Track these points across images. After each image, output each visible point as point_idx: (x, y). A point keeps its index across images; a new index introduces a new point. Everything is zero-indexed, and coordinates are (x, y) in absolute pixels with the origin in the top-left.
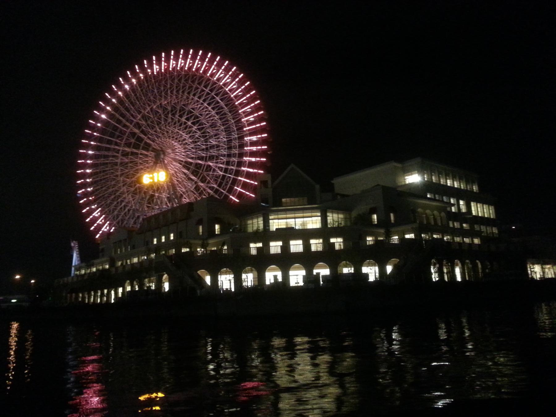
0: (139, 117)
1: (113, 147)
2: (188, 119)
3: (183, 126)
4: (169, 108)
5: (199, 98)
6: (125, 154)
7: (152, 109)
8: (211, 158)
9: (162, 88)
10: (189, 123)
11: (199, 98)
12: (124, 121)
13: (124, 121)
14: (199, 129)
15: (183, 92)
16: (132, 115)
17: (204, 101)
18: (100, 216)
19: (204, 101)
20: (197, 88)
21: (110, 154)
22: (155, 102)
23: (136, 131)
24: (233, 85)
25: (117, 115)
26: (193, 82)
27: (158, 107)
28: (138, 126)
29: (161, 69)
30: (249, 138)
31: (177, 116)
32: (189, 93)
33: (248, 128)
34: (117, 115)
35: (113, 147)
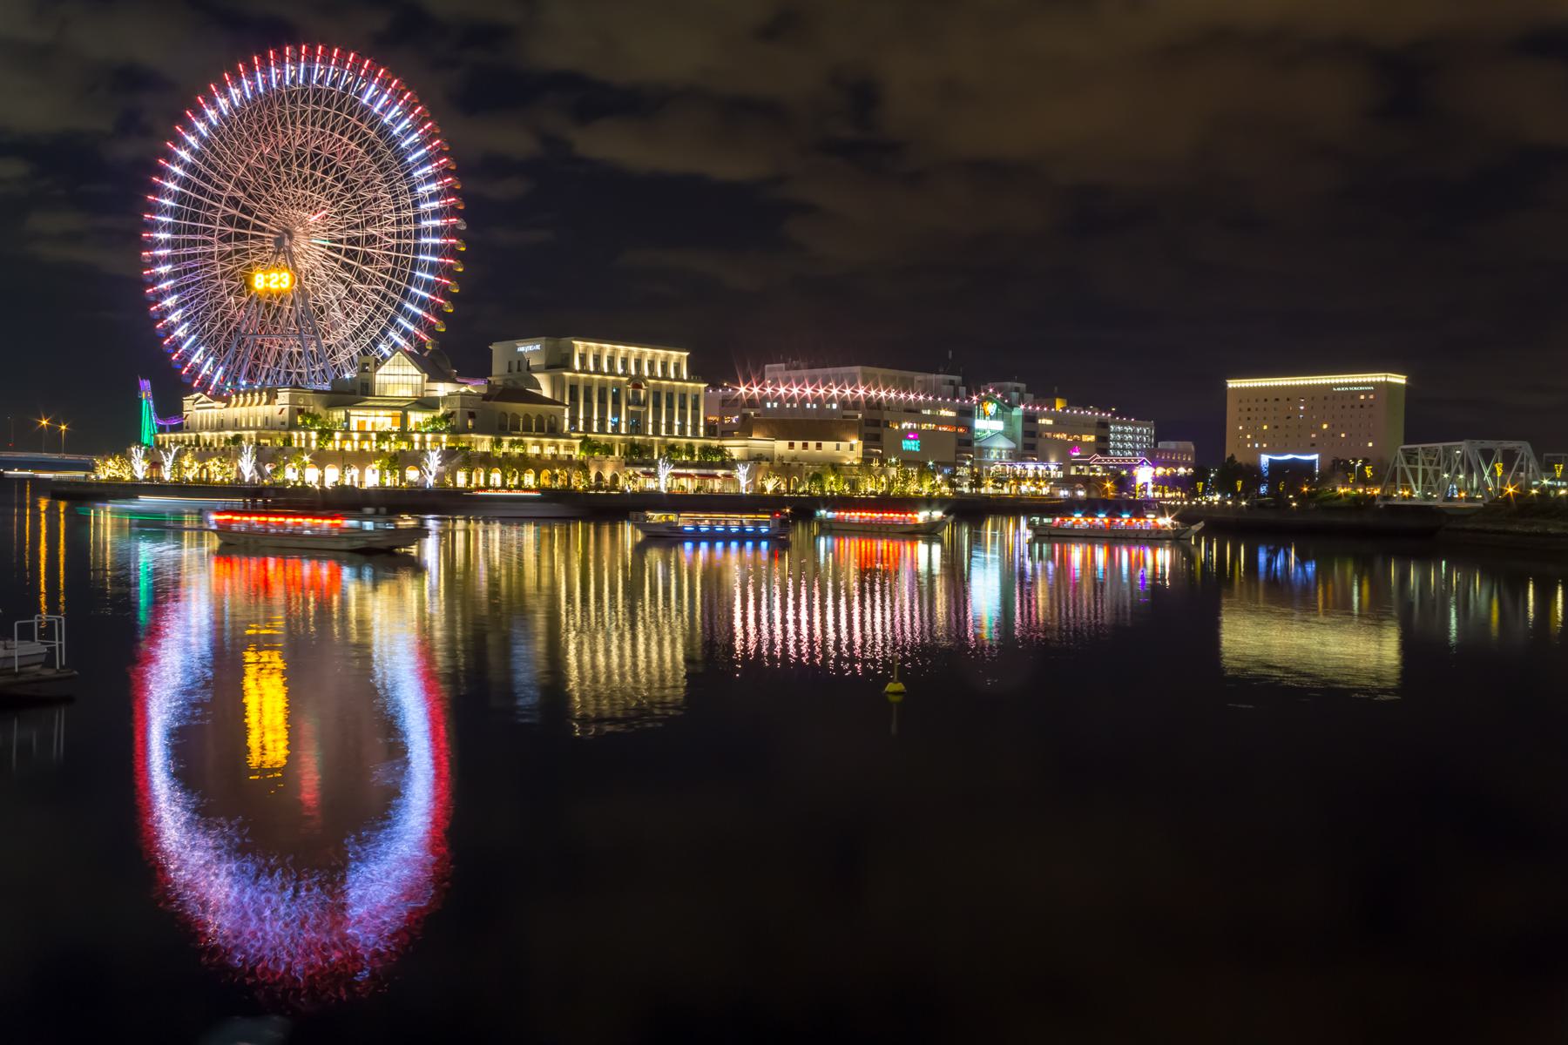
0: (231, 186)
1: (199, 237)
2: (314, 167)
3: (310, 182)
4: (278, 158)
5: (323, 126)
6: (225, 256)
7: (248, 168)
8: (369, 222)
9: (256, 127)
10: (319, 174)
11: (323, 126)
12: (210, 188)
13: (210, 188)
14: (337, 179)
15: (293, 123)
16: (218, 187)
17: (333, 129)
18: (205, 361)
19: (333, 129)
20: (337, 116)
21: (199, 249)
22: (250, 154)
23: (233, 211)
24: (234, 92)
25: (195, 179)
26: (293, 102)
27: (257, 161)
28: (234, 202)
29: (244, 94)
30: (421, 172)
31: (294, 167)
32: (303, 123)
33: (415, 156)
34: (195, 179)
35: (199, 237)
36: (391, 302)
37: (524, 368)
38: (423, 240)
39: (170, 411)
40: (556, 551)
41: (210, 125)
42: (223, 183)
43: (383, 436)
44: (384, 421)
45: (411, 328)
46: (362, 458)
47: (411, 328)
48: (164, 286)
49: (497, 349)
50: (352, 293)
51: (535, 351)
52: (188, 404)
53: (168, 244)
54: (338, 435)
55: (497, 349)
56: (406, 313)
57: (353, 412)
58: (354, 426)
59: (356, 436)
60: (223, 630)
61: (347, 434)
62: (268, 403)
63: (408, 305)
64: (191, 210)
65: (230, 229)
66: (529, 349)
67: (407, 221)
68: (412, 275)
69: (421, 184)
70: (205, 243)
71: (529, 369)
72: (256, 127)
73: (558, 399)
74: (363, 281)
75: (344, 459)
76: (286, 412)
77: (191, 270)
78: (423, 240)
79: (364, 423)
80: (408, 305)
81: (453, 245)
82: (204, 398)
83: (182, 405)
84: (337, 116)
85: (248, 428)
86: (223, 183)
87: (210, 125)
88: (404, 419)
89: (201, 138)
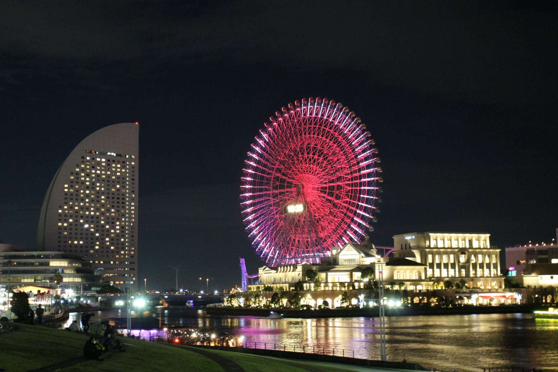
6: (275, 196)
9: (284, 139)
36: (349, 217)
37: (408, 247)
38: (363, 180)
39: (253, 270)
40: (454, 330)
41: (265, 141)
42: (271, 172)
43: (342, 284)
44: (345, 278)
45: (361, 222)
46: (333, 294)
47: (361, 222)
48: (248, 202)
49: (396, 238)
50: (335, 205)
51: (412, 239)
52: (261, 271)
53: (251, 205)
54: (322, 285)
55: (396, 238)
56: (356, 223)
57: (329, 274)
58: (330, 280)
59: (330, 285)
60: (497, 356)
61: (326, 283)
62: (293, 271)
63: (358, 211)
64: (258, 180)
65: (276, 192)
66: (409, 238)
67: (355, 172)
68: (360, 197)
69: (360, 154)
70: (266, 190)
71: (410, 248)
72: (284, 139)
73: (423, 263)
74: (336, 207)
75: (325, 294)
76: (301, 275)
77: (261, 208)
78: (363, 180)
79: (334, 278)
80: (358, 211)
81: (377, 180)
82: (267, 269)
83: (258, 271)
84: (319, 128)
85: (285, 283)
86: (271, 172)
87: (265, 141)
88: (351, 276)
89: (261, 148)
